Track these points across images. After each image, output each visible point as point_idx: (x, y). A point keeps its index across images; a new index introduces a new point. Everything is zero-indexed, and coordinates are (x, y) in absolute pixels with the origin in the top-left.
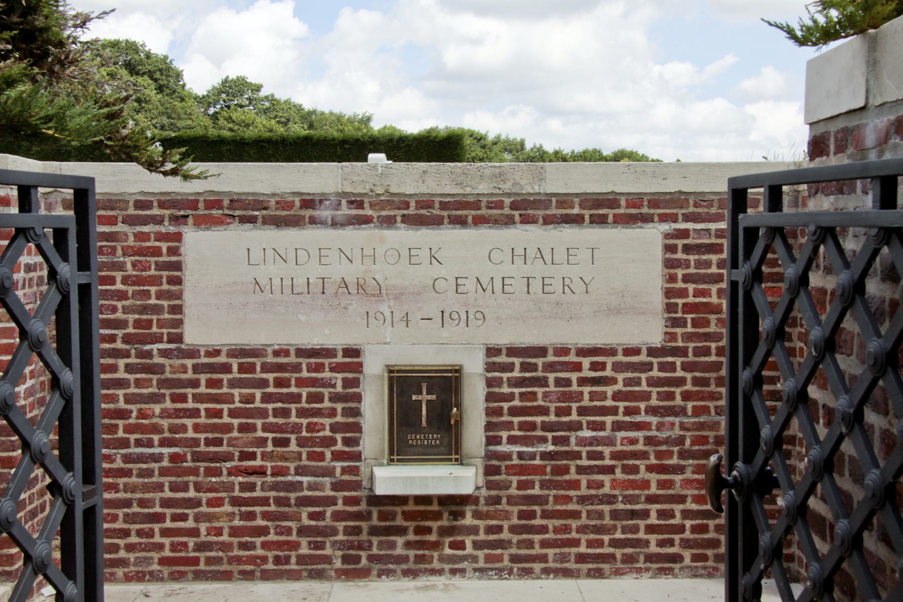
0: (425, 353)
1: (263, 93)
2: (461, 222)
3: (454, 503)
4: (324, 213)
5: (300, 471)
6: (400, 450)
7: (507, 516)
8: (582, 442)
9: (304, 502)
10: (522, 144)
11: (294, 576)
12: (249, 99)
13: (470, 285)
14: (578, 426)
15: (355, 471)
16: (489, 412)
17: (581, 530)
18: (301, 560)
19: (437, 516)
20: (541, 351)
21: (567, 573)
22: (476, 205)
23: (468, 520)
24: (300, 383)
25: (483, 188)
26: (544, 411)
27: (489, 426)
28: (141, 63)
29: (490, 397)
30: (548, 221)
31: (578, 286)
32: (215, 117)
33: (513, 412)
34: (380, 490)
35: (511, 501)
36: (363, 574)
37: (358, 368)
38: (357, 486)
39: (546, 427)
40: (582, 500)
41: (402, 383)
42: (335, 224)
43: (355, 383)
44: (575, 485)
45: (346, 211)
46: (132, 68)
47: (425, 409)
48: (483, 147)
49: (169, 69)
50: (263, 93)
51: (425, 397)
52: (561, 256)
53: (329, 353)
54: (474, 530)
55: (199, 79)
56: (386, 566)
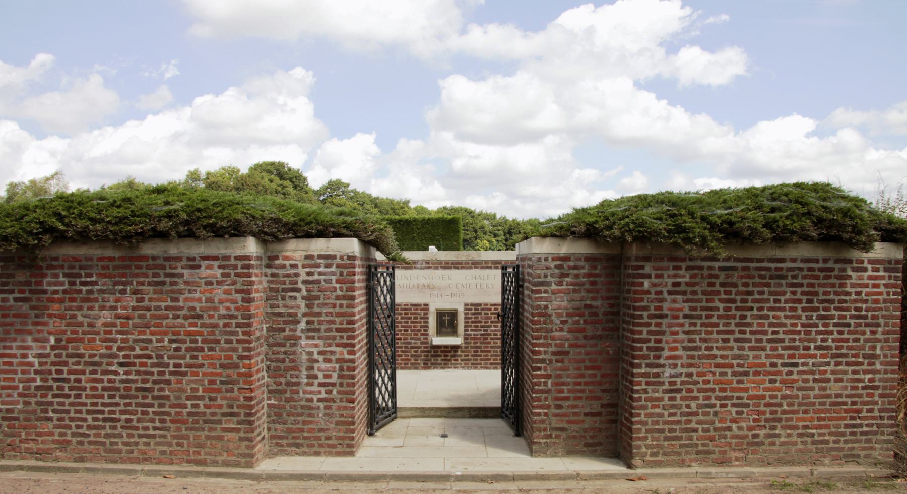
0: (447, 305)
1: (350, 188)
2: (457, 268)
3: (455, 348)
4: (418, 266)
5: (411, 339)
6: (440, 333)
7: (470, 352)
8: (492, 331)
9: (412, 348)
10: (495, 216)
11: (409, 369)
12: (343, 192)
13: (460, 286)
14: (490, 326)
15: (426, 339)
16: (465, 322)
17: (492, 356)
18: (412, 364)
19: (450, 352)
20: (480, 305)
21: (487, 368)
22: (461, 263)
23: (459, 353)
24: (412, 314)
25: (464, 259)
26: (481, 322)
27: (465, 326)
28: (286, 173)
29: (465, 318)
30: (482, 268)
31: (491, 286)
32: (324, 201)
33: (472, 322)
34: (434, 343)
35: (471, 347)
36: (429, 368)
37: (428, 310)
38: (427, 343)
39: (482, 327)
40: (492, 347)
41: (440, 314)
42: (421, 269)
43: (427, 314)
44: (490, 343)
45: (424, 265)
46: (281, 176)
47: (447, 322)
48: (473, 217)
49: (301, 176)
50: (350, 188)
51: (447, 318)
52: (485, 277)
53: (420, 305)
54: (461, 356)
55: (316, 180)
56: (435, 366)
